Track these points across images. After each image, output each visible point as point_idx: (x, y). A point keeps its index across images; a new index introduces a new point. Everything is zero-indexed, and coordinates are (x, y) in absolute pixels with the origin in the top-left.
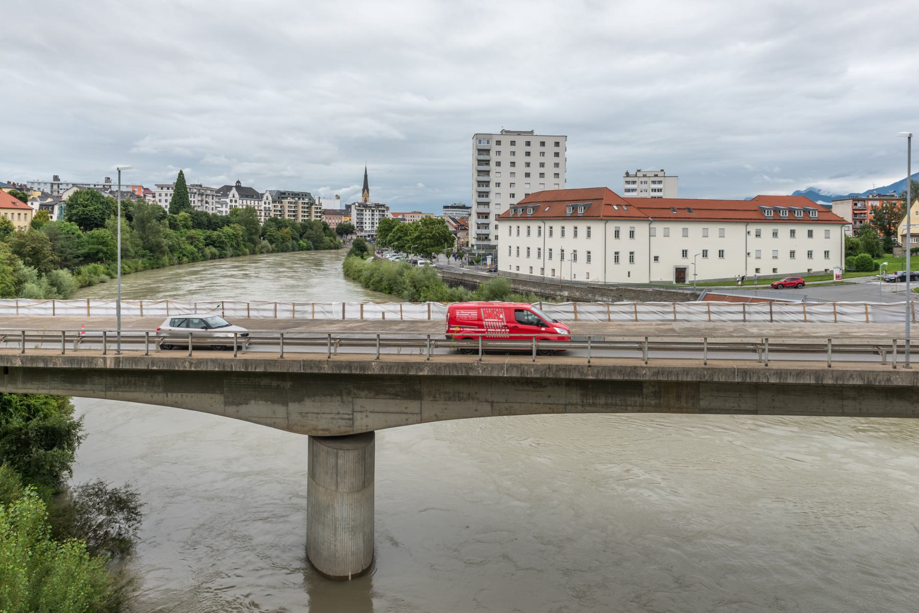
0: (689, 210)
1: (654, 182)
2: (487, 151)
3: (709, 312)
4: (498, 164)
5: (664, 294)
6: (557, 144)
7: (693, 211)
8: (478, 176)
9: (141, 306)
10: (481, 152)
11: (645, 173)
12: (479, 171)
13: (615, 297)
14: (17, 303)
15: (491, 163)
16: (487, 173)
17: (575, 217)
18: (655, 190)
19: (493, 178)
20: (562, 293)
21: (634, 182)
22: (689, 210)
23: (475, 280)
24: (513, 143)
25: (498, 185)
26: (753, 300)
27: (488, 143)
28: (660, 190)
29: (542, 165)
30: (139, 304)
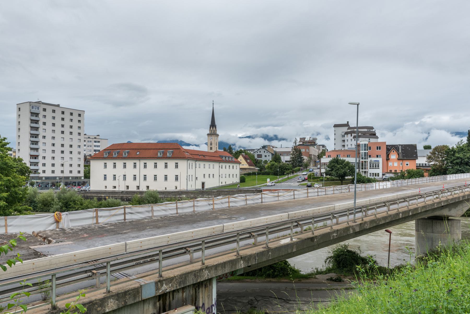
1: (95, 142)
2: (37, 115)
4: (44, 124)
5: (242, 191)
6: (80, 115)
9: (326, 190)
11: (89, 136)
13: (216, 195)
14: (278, 194)
16: (37, 129)
17: (164, 157)
18: (96, 146)
19: (41, 132)
20: (181, 196)
22: (204, 156)
23: (99, 195)
25: (44, 137)
27: (38, 109)
28: (98, 146)
29: (71, 127)
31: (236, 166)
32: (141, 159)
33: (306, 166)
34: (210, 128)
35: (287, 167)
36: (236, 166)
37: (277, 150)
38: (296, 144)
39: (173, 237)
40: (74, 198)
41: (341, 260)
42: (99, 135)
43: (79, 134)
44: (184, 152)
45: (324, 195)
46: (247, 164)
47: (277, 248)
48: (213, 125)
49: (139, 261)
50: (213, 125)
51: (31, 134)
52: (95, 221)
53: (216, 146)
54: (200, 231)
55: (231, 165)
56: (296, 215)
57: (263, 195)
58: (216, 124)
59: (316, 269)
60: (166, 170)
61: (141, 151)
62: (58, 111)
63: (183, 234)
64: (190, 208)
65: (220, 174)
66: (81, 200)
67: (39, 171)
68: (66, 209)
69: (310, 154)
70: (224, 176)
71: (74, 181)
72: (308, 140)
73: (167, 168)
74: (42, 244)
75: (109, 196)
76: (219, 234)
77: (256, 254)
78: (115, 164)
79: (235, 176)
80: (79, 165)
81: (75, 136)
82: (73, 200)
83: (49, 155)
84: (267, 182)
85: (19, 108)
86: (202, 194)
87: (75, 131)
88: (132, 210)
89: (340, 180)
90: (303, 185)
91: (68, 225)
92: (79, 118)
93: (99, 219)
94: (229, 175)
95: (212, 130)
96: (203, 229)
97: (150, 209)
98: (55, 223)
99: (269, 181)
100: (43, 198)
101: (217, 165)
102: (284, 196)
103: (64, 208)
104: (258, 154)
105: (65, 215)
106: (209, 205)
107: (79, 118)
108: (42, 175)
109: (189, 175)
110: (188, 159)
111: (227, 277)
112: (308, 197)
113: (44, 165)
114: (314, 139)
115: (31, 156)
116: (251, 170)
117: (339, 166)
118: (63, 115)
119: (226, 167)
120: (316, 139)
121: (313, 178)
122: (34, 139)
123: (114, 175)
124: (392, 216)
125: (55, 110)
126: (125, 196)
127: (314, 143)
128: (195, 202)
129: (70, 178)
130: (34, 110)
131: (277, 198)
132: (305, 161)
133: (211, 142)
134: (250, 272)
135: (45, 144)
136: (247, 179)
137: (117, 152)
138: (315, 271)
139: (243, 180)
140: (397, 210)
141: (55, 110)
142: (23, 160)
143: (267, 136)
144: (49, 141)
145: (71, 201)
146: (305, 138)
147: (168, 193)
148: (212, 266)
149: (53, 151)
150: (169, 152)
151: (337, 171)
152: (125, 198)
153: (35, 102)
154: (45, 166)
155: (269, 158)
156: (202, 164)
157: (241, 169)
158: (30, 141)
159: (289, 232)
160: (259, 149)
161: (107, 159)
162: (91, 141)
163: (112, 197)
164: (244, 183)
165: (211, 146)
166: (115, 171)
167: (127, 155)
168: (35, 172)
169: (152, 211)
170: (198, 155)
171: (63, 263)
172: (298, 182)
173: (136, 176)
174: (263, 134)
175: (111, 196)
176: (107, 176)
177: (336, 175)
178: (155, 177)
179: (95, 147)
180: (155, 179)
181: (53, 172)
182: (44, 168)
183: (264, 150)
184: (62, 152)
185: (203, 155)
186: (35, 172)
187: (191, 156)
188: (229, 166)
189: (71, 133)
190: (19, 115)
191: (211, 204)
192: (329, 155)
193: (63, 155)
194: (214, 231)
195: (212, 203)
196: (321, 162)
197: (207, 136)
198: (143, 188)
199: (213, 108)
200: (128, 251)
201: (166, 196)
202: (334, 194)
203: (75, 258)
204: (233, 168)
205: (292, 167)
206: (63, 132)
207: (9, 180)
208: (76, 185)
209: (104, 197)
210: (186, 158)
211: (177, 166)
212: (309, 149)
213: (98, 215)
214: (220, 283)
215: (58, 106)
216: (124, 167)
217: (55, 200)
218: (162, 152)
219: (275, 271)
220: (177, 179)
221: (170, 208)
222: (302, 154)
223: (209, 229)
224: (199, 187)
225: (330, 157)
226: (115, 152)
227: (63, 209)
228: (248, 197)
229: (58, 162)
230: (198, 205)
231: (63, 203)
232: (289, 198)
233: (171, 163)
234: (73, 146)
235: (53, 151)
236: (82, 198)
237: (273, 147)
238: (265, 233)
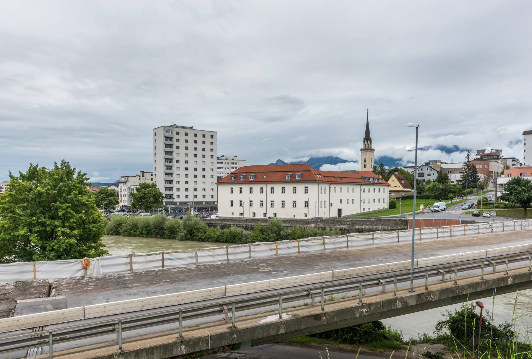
1: (233, 163)
2: (171, 139)
4: (178, 147)
6: (212, 137)
9: (451, 230)
10: (167, 139)
11: (227, 158)
14: (373, 236)
15: (173, 146)
17: (293, 181)
18: (234, 168)
19: (175, 157)
20: (309, 226)
21: (222, 163)
22: (341, 178)
23: (224, 223)
24: (187, 134)
25: (178, 161)
27: (172, 133)
29: (204, 149)
30: (450, 228)
32: (269, 183)
33: (482, 187)
34: (364, 142)
35: (453, 188)
36: (384, 189)
37: (444, 166)
38: (468, 158)
39: (150, 301)
40: (198, 226)
41: (457, 327)
42: (236, 156)
44: (315, 174)
45: (448, 236)
46: (401, 186)
47: (247, 329)
48: (367, 138)
49: (44, 340)
50: (367, 138)
51: (166, 159)
52: (128, 267)
53: (371, 163)
54: (189, 294)
56: (347, 273)
57: (349, 238)
59: (424, 335)
60: (295, 195)
61: (268, 174)
62: (191, 133)
63: (164, 297)
66: (205, 227)
68: (190, 236)
69: (490, 171)
70: (367, 201)
71: (207, 206)
72: (490, 152)
73: (296, 192)
74: (41, 297)
76: (219, 297)
77: (208, 336)
79: (381, 201)
80: (212, 190)
81: (208, 159)
83: (182, 179)
84: (420, 210)
85: (155, 133)
86: (333, 223)
87: (208, 153)
88: (171, 256)
89: (523, 207)
90: (468, 213)
91: (99, 273)
92: (212, 140)
93: (133, 265)
94: (374, 200)
95: (366, 145)
96: (194, 292)
97: (194, 254)
98: (83, 269)
99: (423, 208)
100: (170, 225)
101: (357, 188)
104: (419, 172)
105: (96, 261)
106: (271, 250)
107: (212, 140)
108: (176, 200)
109: (321, 201)
110: (318, 182)
111: (224, 350)
112: (438, 237)
113: (178, 190)
114: (497, 151)
115: (166, 181)
116: (406, 193)
117: (520, 189)
119: (369, 190)
120: (501, 151)
121: (485, 204)
122: (168, 164)
124: (491, 283)
126: (249, 224)
127: (498, 156)
128: (252, 247)
129: (204, 203)
130: (168, 135)
131: (372, 240)
132: (481, 180)
133: (365, 159)
134: (323, 333)
136: (400, 204)
137: (243, 176)
138: (419, 339)
139: (393, 205)
140: (505, 273)
142: (157, 186)
143: (445, 147)
144: (182, 165)
145: (195, 229)
146: (484, 150)
147: (294, 222)
148: (131, 352)
149: (187, 176)
150: (297, 175)
151: (518, 195)
152: (249, 226)
153: (169, 126)
155: (434, 177)
156: (338, 187)
159: (277, 306)
161: (233, 184)
163: (236, 225)
165: (365, 163)
167: (253, 179)
168: (170, 197)
169: (196, 257)
171: (4, 329)
172: (463, 209)
174: (439, 145)
175: (236, 223)
176: (297, 203)
177: (515, 201)
179: (232, 169)
181: (187, 197)
183: (427, 167)
184: (196, 176)
185: (340, 177)
186: (170, 197)
187: (324, 179)
188: (374, 189)
190: (155, 140)
191: (274, 249)
192: (509, 173)
193: (196, 180)
194: (211, 294)
195: (275, 247)
196: (498, 183)
197: (360, 151)
199: (368, 118)
200: (87, 316)
201: (292, 225)
202: (465, 235)
203: (19, 323)
204: (379, 191)
205: (461, 189)
207: (80, 217)
210: (317, 181)
211: (306, 191)
212: (488, 165)
213: (133, 261)
214: (277, 345)
215: (192, 128)
217: (180, 228)
218: (290, 174)
219: (355, 335)
221: (219, 253)
222: (476, 172)
223: (203, 292)
225: (511, 176)
226: (241, 176)
228: (326, 241)
229: (191, 186)
230: (256, 250)
231: (188, 231)
232: (391, 241)
233: (300, 188)
234: (206, 170)
235: (187, 176)
237: (442, 163)
238: (278, 301)
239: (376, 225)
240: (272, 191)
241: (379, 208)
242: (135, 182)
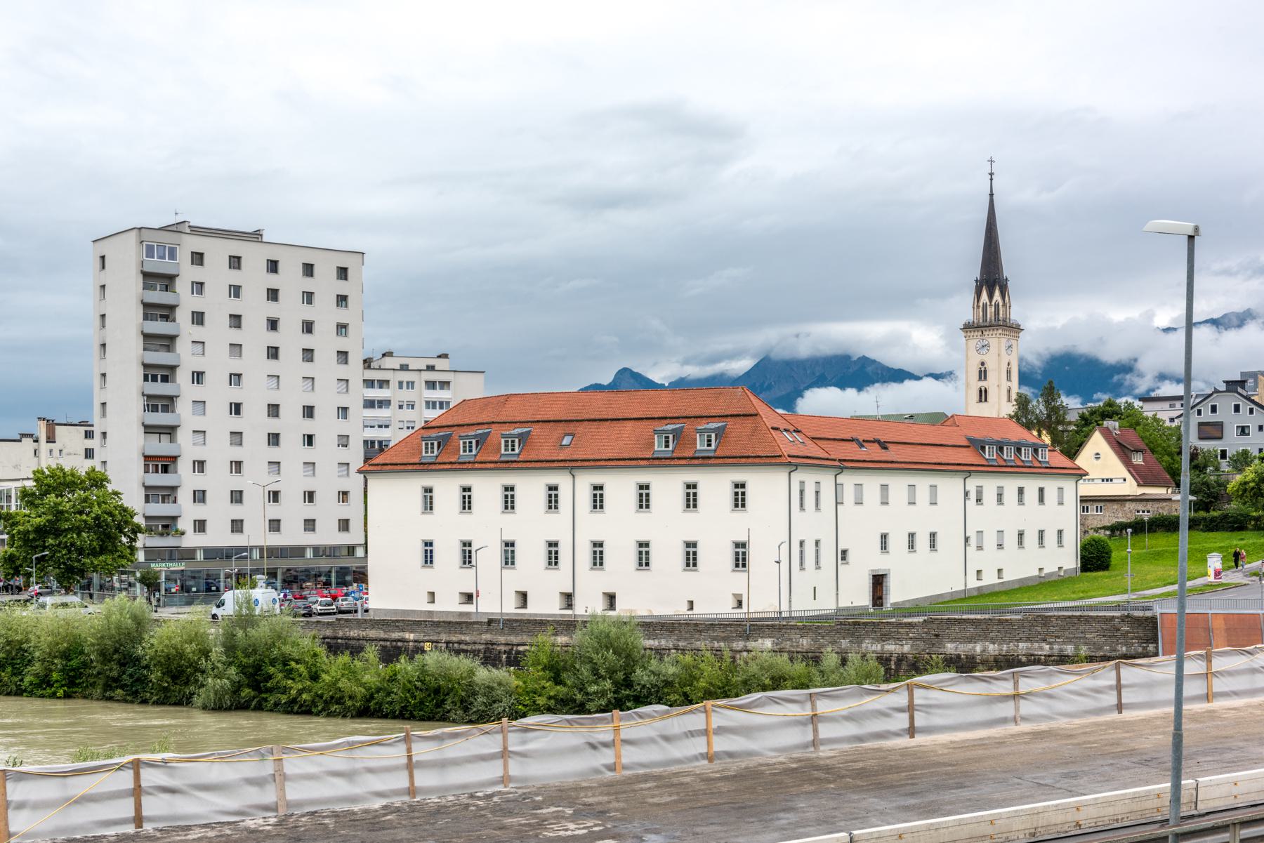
0: (884, 445)
1: (431, 385)
2: (168, 281)
3: (814, 719)
4: (198, 318)
6: (343, 273)
7: (890, 446)
8: (145, 349)
10: (150, 282)
11: (404, 361)
12: (147, 336)
16: (168, 342)
18: (434, 403)
19: (185, 357)
20: (751, 645)
21: (383, 383)
22: (884, 445)
23: (396, 635)
24: (235, 262)
25: (198, 377)
26: (1034, 660)
27: (172, 255)
29: (308, 327)
31: (1060, 489)
34: (978, 294)
36: (1060, 489)
40: (287, 649)
43: (343, 356)
53: (1005, 384)
55: (1031, 486)
57: (918, 693)
58: (1006, 272)
60: (691, 515)
61: (581, 429)
64: (484, 764)
65: (971, 533)
67: (181, 525)
70: (990, 541)
71: (324, 564)
75: (435, 638)
78: (467, 494)
79: (1051, 538)
80: (344, 495)
82: (283, 655)
83: (218, 452)
84: (1206, 575)
86: (853, 635)
87: (325, 342)
88: (171, 776)
94: (1021, 534)
100: (167, 646)
102: (1050, 696)
103: (247, 690)
104: (1203, 419)
106: (593, 746)
108: (191, 540)
109: (802, 543)
110: (790, 464)
112: (1120, 707)
113: (200, 496)
118: (273, 276)
122: (159, 388)
123: (464, 544)
125: (239, 258)
126: (502, 639)
129: (309, 554)
130: (158, 265)
133: (983, 364)
135: (202, 405)
136: (1124, 551)
139: (1098, 558)
141: (239, 258)
142: (108, 481)
144: (217, 392)
145: (273, 663)
149: (237, 437)
150: (701, 432)
152: (503, 648)
153: (160, 229)
154: (203, 500)
156: (871, 483)
157: (1085, 500)
158: (143, 395)
160: (1210, 395)
162: (413, 383)
164: (1100, 573)
165: (983, 384)
166: (468, 526)
170: (852, 440)
173: (556, 544)
175: (444, 637)
176: (436, 548)
178: (641, 553)
179: (428, 407)
180: (640, 559)
181: (237, 526)
182: (199, 512)
183: (1233, 399)
184: (274, 439)
185: (878, 442)
187: (813, 450)
188: (1021, 491)
189: (308, 354)
191: (606, 745)
193: (274, 453)
198: (589, 605)
199: (991, 195)
201: (681, 644)
204: (1041, 500)
206: (273, 353)
208: (330, 584)
209: (415, 641)
215: (256, 236)
216: (506, 508)
217: (213, 656)
220: (741, 560)
224: (858, 596)
227: (243, 694)
228: (824, 707)
229: (254, 481)
230: (531, 746)
231: (243, 669)
236: (318, 650)
239: (1028, 639)
240: (598, 502)
241: (1041, 569)
242: (16, 467)
